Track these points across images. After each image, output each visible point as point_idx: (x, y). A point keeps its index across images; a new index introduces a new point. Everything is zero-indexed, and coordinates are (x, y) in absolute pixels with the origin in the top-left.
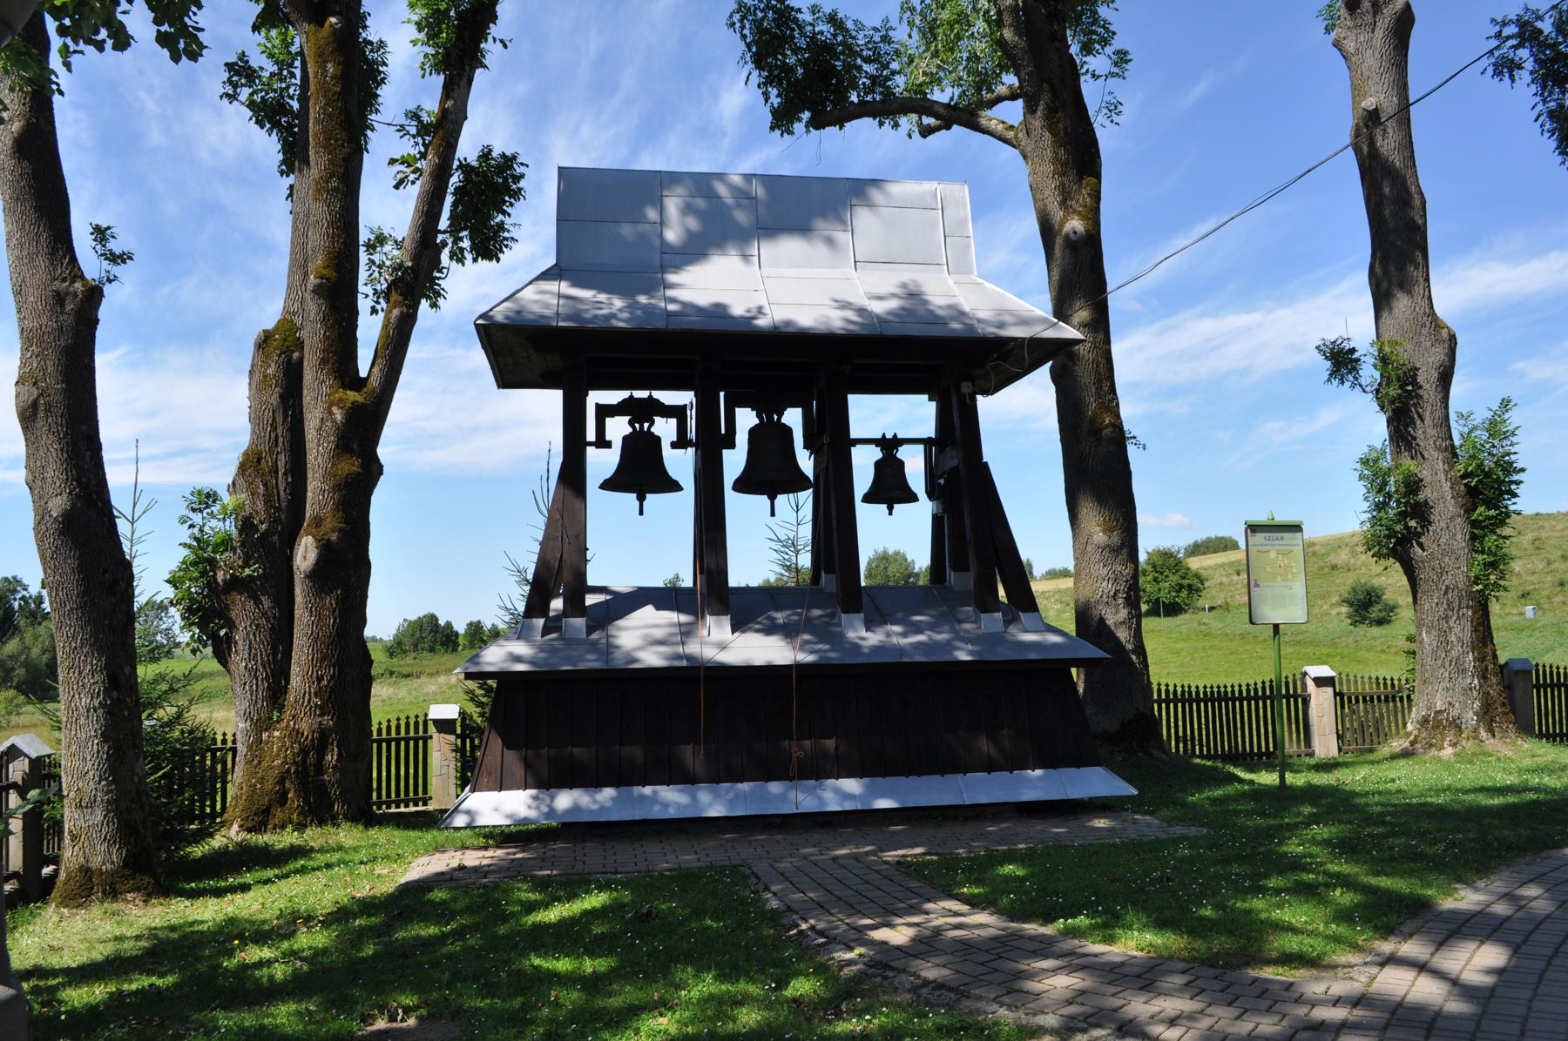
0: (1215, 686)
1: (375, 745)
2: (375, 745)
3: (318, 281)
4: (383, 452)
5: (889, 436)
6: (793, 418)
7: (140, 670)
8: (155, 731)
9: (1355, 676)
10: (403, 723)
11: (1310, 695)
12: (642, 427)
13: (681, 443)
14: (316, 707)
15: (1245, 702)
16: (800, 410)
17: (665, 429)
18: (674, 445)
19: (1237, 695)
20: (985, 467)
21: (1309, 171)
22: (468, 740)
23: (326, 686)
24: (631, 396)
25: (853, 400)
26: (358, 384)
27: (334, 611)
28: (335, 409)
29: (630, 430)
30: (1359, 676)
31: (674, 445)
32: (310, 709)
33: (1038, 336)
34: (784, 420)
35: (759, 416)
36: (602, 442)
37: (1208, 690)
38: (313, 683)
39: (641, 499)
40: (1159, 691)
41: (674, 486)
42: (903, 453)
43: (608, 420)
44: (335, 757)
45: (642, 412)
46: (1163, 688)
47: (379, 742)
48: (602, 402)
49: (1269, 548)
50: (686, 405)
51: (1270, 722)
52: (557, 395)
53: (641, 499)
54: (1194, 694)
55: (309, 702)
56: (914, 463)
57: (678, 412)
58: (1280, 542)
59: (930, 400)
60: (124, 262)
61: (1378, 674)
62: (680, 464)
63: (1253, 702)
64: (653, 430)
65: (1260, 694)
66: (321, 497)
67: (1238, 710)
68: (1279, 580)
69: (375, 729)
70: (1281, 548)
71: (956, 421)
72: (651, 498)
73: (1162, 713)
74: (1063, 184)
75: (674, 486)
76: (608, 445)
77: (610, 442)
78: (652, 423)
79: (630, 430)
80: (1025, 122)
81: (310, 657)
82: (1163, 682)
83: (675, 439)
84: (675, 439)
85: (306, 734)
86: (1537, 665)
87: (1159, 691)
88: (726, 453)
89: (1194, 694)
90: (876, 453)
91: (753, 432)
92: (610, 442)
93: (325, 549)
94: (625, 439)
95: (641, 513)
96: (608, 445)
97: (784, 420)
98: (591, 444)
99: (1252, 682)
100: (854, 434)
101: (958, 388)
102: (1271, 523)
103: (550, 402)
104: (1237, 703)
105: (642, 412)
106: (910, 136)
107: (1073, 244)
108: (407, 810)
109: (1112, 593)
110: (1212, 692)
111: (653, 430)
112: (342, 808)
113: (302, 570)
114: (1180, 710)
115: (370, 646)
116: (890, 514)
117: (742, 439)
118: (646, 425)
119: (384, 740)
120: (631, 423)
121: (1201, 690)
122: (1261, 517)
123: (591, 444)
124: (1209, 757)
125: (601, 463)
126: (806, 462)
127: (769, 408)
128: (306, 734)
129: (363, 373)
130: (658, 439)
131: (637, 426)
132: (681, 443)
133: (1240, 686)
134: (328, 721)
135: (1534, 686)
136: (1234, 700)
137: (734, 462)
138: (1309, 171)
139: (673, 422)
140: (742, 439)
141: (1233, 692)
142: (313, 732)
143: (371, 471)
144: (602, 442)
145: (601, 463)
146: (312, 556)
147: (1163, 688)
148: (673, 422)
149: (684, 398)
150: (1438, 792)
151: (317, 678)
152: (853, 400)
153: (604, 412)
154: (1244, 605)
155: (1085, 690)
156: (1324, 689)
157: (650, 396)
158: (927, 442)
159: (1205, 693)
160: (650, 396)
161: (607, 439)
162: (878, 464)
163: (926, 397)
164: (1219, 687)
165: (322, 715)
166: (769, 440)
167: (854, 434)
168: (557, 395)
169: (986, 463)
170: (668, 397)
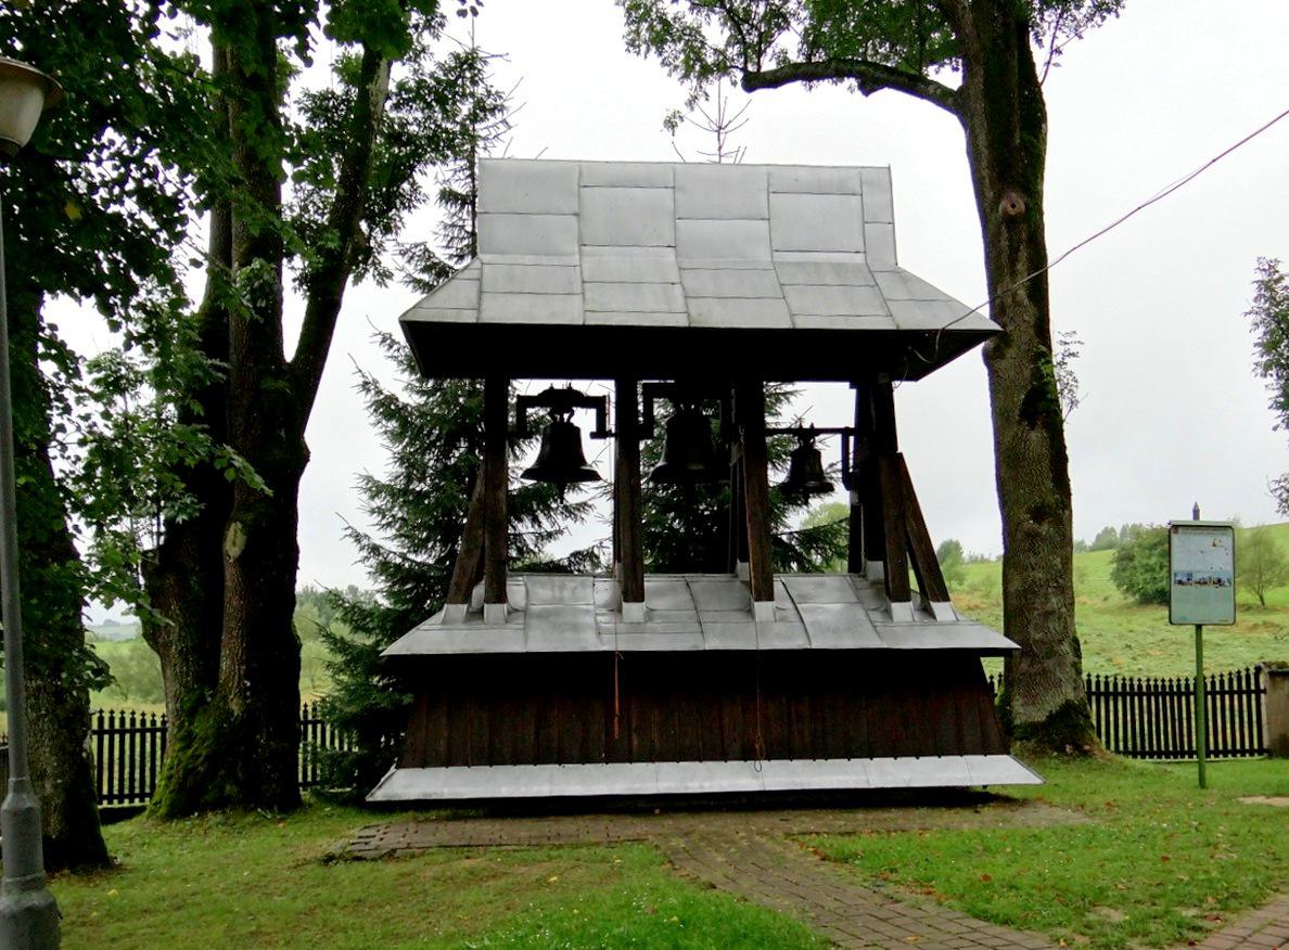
0: (1167, 679)
4: (312, 435)
5: (806, 425)
13: (600, 433)
15: (1145, 698)
17: (584, 419)
18: (593, 436)
19: (1175, 690)
21: (1214, 161)
31: (593, 436)
33: (950, 327)
35: (676, 406)
54: (1136, 687)
56: (830, 452)
57: (598, 403)
60: (434, 37)
63: (1168, 698)
64: (572, 420)
71: (873, 413)
75: (593, 476)
78: (572, 414)
82: (1103, 674)
83: (594, 430)
84: (594, 430)
86: (1239, 672)
89: (1136, 687)
93: (253, 535)
99: (1226, 673)
104: (1168, 698)
107: (1011, 222)
113: (232, 555)
114: (1254, 703)
118: (566, 416)
130: (577, 430)
132: (600, 433)
133: (1179, 680)
135: (94, 732)
136: (1107, 694)
138: (1214, 161)
139: (592, 412)
146: (241, 539)
148: (592, 412)
149: (604, 388)
158: (845, 432)
164: (1163, 681)
169: (901, 454)
170: (582, 386)
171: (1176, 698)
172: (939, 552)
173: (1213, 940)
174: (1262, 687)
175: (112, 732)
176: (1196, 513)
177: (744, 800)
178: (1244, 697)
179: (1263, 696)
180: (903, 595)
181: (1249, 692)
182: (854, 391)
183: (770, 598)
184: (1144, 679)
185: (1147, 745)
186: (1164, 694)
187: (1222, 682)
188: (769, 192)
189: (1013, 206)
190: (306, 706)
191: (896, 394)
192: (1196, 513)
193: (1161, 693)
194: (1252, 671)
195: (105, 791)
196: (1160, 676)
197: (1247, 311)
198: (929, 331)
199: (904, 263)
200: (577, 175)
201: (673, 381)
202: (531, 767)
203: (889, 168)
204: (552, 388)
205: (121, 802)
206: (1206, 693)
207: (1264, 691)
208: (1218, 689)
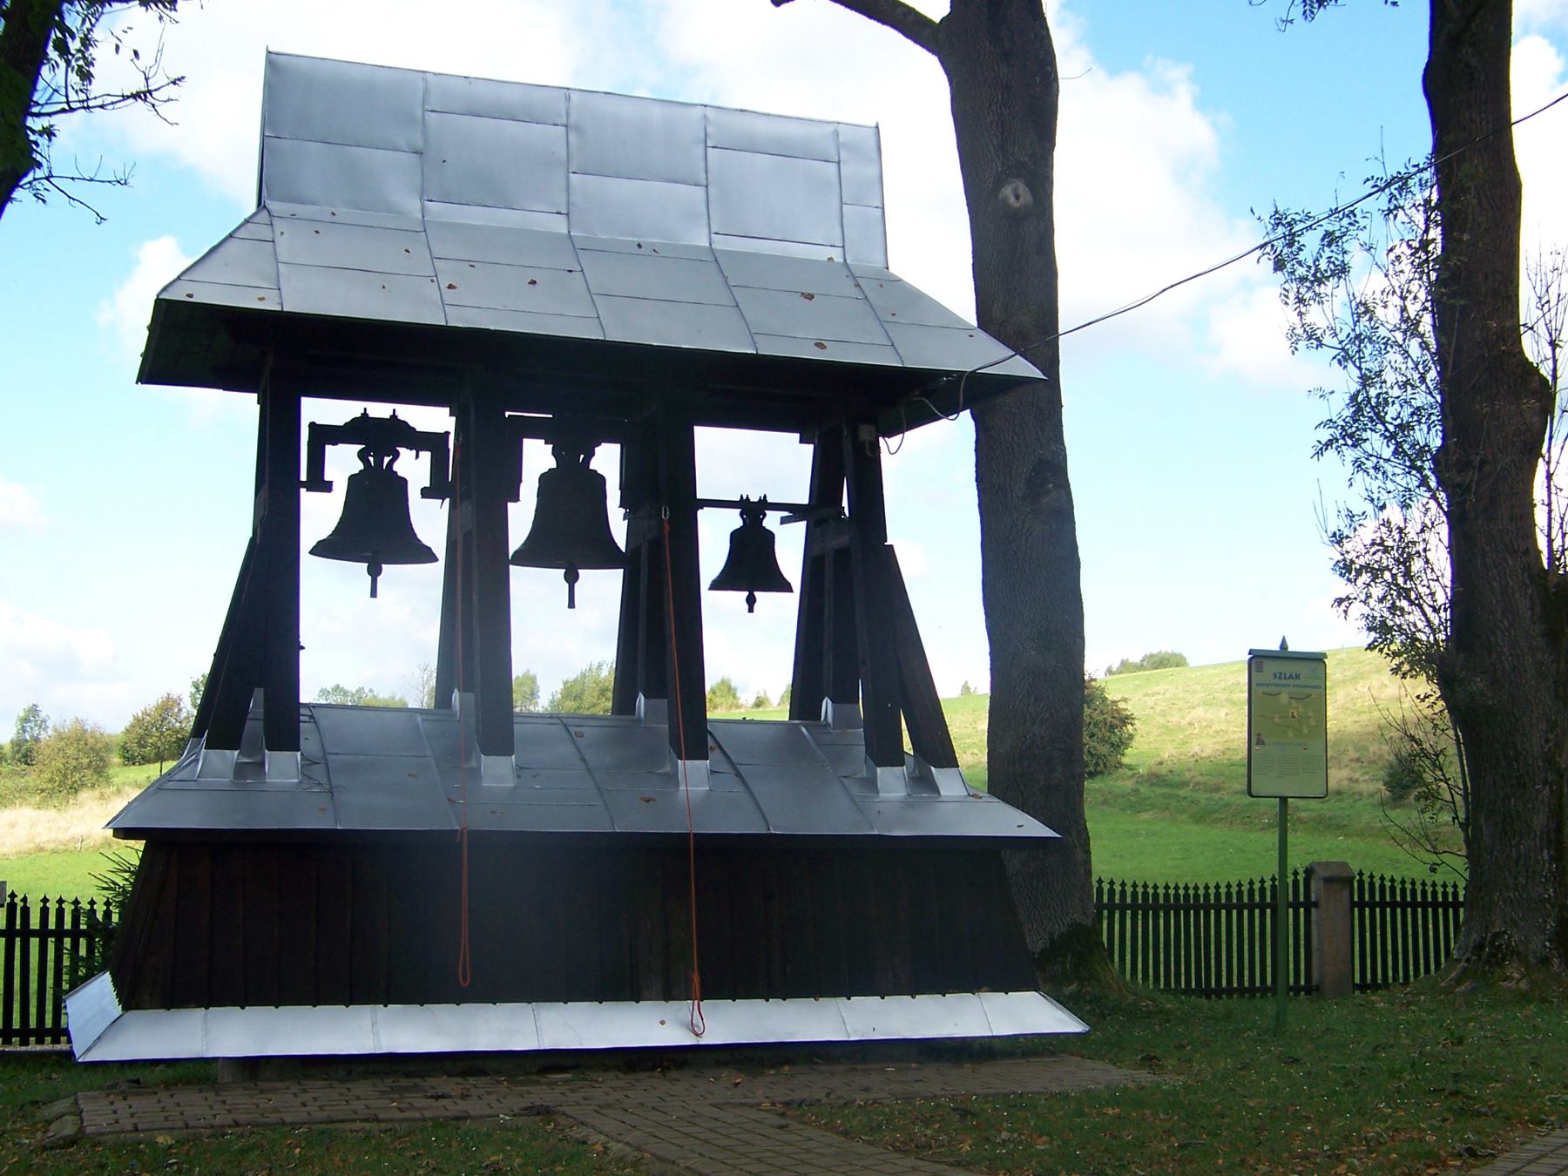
0: (1191, 886)
6: (607, 460)
7: (1436, 442)
12: (379, 461)
17: (413, 467)
18: (426, 493)
20: (337, 444)
24: (365, 414)
29: (361, 466)
31: (426, 493)
34: (594, 465)
36: (320, 484)
37: (1172, 892)
40: (1100, 890)
41: (424, 555)
42: (771, 521)
43: (330, 450)
48: (321, 421)
50: (447, 433)
51: (1235, 935)
54: (1212, 897)
57: (431, 442)
58: (1297, 682)
59: (801, 441)
65: (1246, 900)
67: (1410, 940)
68: (1291, 734)
70: (1297, 690)
76: (327, 487)
77: (331, 483)
78: (396, 456)
79: (361, 466)
86: (76, 902)
88: (510, 505)
90: (733, 519)
91: (545, 479)
92: (331, 483)
94: (352, 479)
96: (327, 487)
97: (594, 465)
98: (303, 484)
100: (700, 495)
101: (855, 437)
103: (243, 409)
104: (1246, 912)
108: (39, 1048)
116: (751, 610)
118: (387, 460)
120: (362, 456)
123: (303, 484)
130: (404, 482)
137: (521, 519)
139: (426, 456)
141: (1207, 895)
144: (320, 484)
148: (426, 456)
149: (434, 419)
153: (324, 435)
154: (1243, 776)
155: (1464, 919)
157: (394, 416)
159: (1445, 894)
160: (394, 416)
162: (735, 536)
163: (797, 436)
167: (700, 495)
171: (1451, 911)
172: (517, 678)
174: (1313, 898)
176: (751, 601)
179: (1313, 910)
180: (893, 756)
182: (809, 449)
183: (293, 745)
185: (1369, 976)
186: (1123, 908)
187: (1251, 891)
188: (706, 146)
189: (1017, 197)
190: (1296, 873)
191: (444, 409)
192: (751, 601)
196: (1408, 876)
197: (52, 170)
198: (948, 373)
199: (895, 269)
200: (420, 95)
202: (340, 1009)
203: (877, 127)
206: (1353, 904)
207: (1316, 904)
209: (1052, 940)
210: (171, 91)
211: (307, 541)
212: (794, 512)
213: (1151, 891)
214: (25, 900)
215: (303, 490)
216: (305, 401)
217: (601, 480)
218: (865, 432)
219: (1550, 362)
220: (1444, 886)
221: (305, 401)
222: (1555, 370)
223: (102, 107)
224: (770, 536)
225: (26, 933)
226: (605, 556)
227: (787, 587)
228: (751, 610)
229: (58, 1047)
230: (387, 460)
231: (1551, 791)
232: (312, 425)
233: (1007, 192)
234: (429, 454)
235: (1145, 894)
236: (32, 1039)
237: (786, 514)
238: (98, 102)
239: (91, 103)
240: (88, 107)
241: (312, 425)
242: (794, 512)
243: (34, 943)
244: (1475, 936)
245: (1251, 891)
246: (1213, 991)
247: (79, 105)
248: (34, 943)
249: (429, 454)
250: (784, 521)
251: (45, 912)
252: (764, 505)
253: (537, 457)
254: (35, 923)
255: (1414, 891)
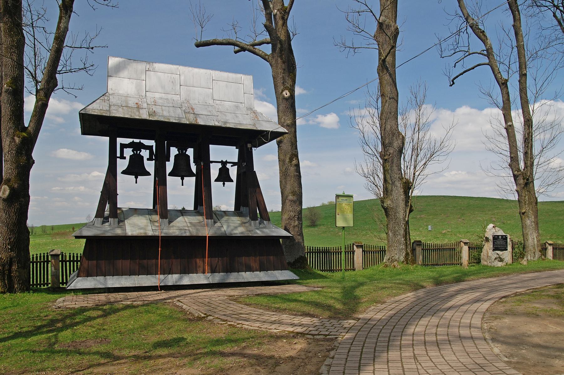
1: (31, 264)
2: (31, 264)
3: (8, 88)
4: (34, 155)
5: (224, 161)
6: (190, 152)
8: (444, 240)
9: (374, 246)
10: (39, 256)
11: (355, 251)
12: (137, 152)
14: (8, 249)
16: (193, 149)
17: (145, 154)
18: (148, 159)
22: (64, 263)
23: (13, 242)
24: (133, 141)
25: (211, 147)
26: (25, 129)
27: (16, 214)
28: (16, 138)
30: (377, 246)
31: (148, 159)
32: (6, 249)
36: (122, 157)
38: (7, 240)
39: (136, 178)
40: (33, 258)
41: (148, 174)
42: (228, 166)
44: (16, 267)
45: (137, 147)
46: (75, 255)
47: (33, 263)
49: (343, 203)
50: (153, 146)
52: (107, 139)
53: (136, 178)
55: (6, 247)
57: (150, 148)
61: (372, 244)
62: (150, 166)
63: (75, 263)
64: (141, 153)
66: (10, 171)
69: (31, 257)
72: (186, 179)
73: (308, 256)
74: (283, 77)
75: (148, 174)
76: (125, 158)
78: (141, 151)
80: (272, 54)
81: (6, 231)
85: (4, 259)
87: (33, 258)
88: (167, 162)
90: (220, 165)
94: (131, 156)
95: (136, 183)
96: (125, 158)
98: (118, 157)
101: (247, 146)
102: (344, 195)
105: (137, 147)
106: (107, 47)
109: (293, 216)
110: (324, 249)
111: (141, 153)
112: (19, 286)
115: (29, 228)
116: (224, 186)
117: (172, 159)
118: (138, 152)
119: (39, 262)
120: (133, 151)
121: (321, 249)
122: (341, 193)
123: (118, 157)
124: (321, 270)
125: (122, 165)
126: (194, 168)
127: (182, 149)
128: (4, 259)
129: (26, 125)
130: (143, 157)
131: (135, 152)
133: (313, 247)
134: (13, 254)
135: (60, 261)
137: (170, 166)
139: (148, 151)
140: (172, 159)
142: (7, 258)
143: (30, 162)
144: (122, 157)
145: (122, 165)
147: (75, 255)
148: (148, 151)
149: (152, 143)
150: (216, 290)
151: (9, 238)
152: (211, 147)
153: (123, 146)
156: (359, 249)
157: (140, 142)
159: (322, 250)
160: (140, 142)
161: (124, 156)
162: (220, 169)
165: (11, 251)
166: (182, 159)
168: (107, 139)
170: (146, 142)
173: (423, 322)
175: (74, 261)
176: (224, 184)
177: (242, 285)
178: (72, 263)
181: (44, 262)
182: (238, 150)
184: (316, 247)
187: (37, 257)
189: (286, 94)
192: (224, 184)
193: (314, 252)
194: (352, 245)
195: (61, 281)
201: (166, 142)
204: (133, 141)
205: (44, 286)
208: (72, 259)
209: (295, 259)
210: (91, 68)
211: (167, 173)
212: (234, 164)
213: (319, 249)
214: (65, 254)
215: (118, 159)
216: (118, 139)
217: (189, 157)
218: (249, 146)
219: (101, 98)
220: (320, 248)
221: (118, 139)
222: (405, 133)
223: (74, 72)
224: (228, 169)
225: (66, 262)
226: (191, 174)
227: (232, 181)
228: (224, 186)
229: (44, 287)
230: (138, 152)
231: (404, 226)
232: (121, 144)
233: (284, 93)
234: (149, 151)
235: (318, 249)
236: (42, 286)
237: (232, 164)
238: (74, 70)
239: (72, 71)
240: (71, 72)
241: (121, 144)
242: (234, 164)
243: (68, 263)
244: (388, 257)
245: (37, 257)
246: (324, 270)
247: (69, 71)
248: (68, 263)
249: (149, 151)
250: (232, 166)
251: (70, 256)
252: (227, 162)
253: (174, 151)
254: (68, 259)
255: (313, 249)
